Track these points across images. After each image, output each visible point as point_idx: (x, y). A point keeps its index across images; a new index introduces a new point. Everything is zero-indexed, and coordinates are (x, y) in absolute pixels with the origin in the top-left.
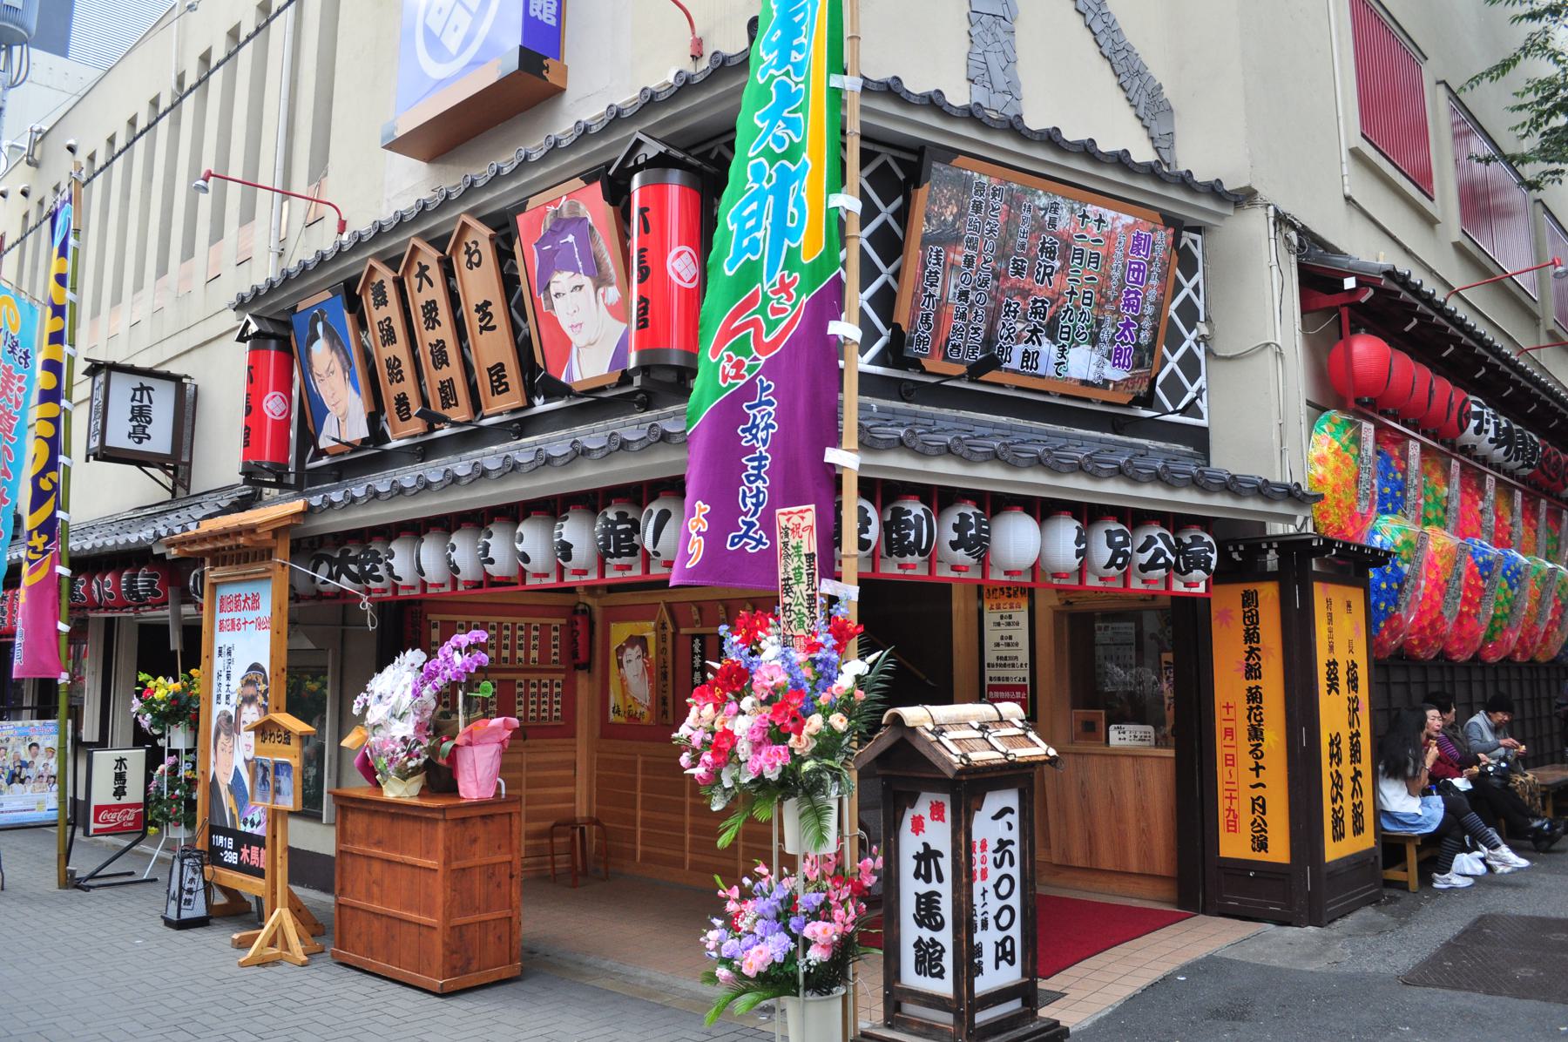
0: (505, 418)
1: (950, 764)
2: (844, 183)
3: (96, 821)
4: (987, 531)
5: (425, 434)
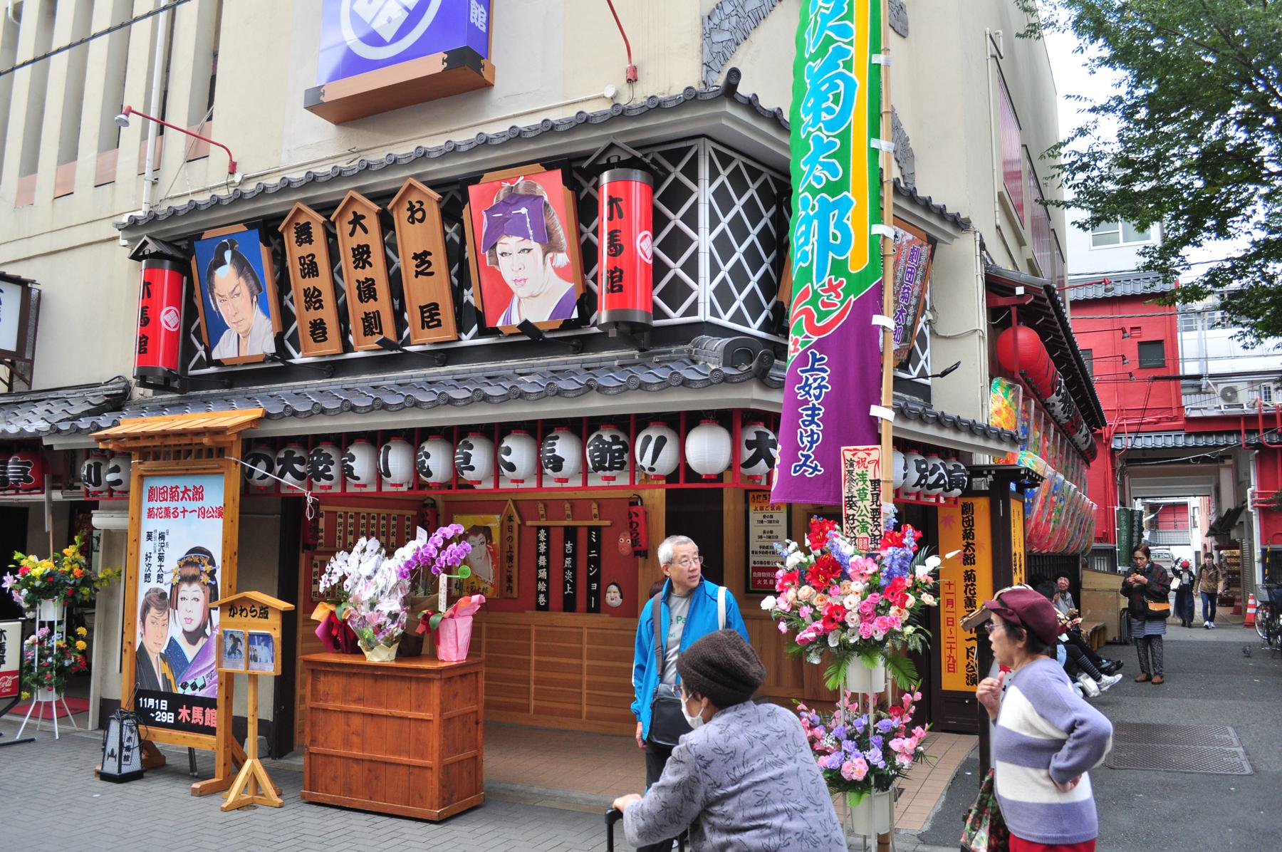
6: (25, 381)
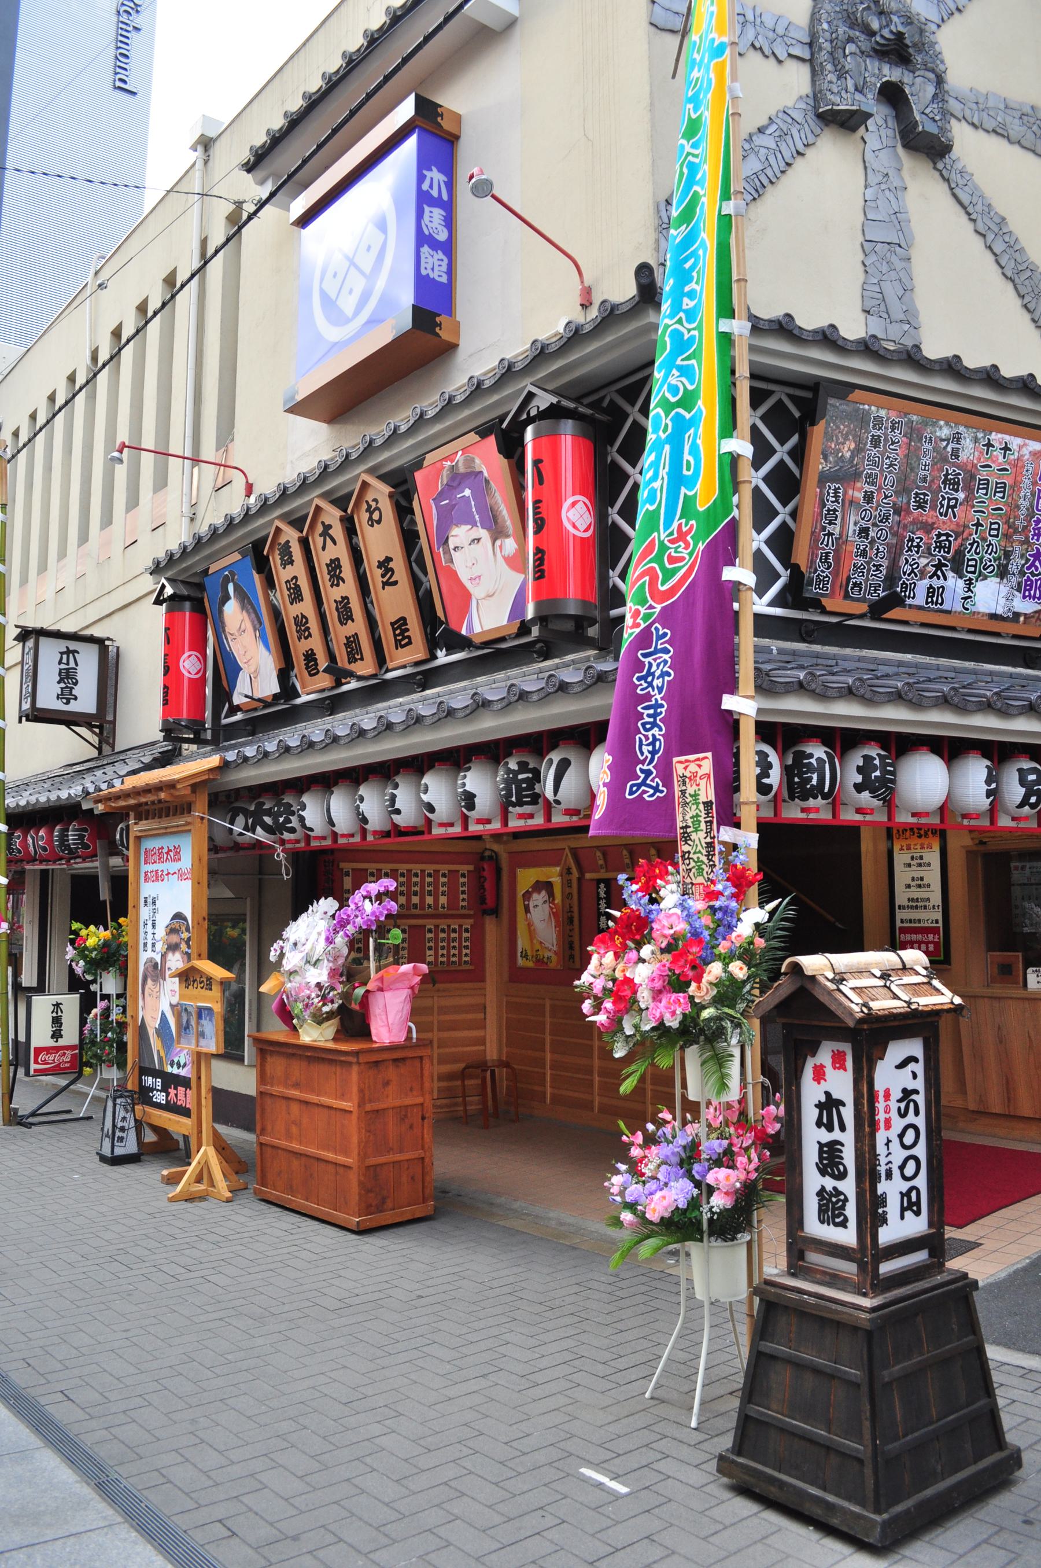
0: (409, 671)
1: (851, 1013)
2: (735, 427)
3: (36, 1062)
5: (332, 688)
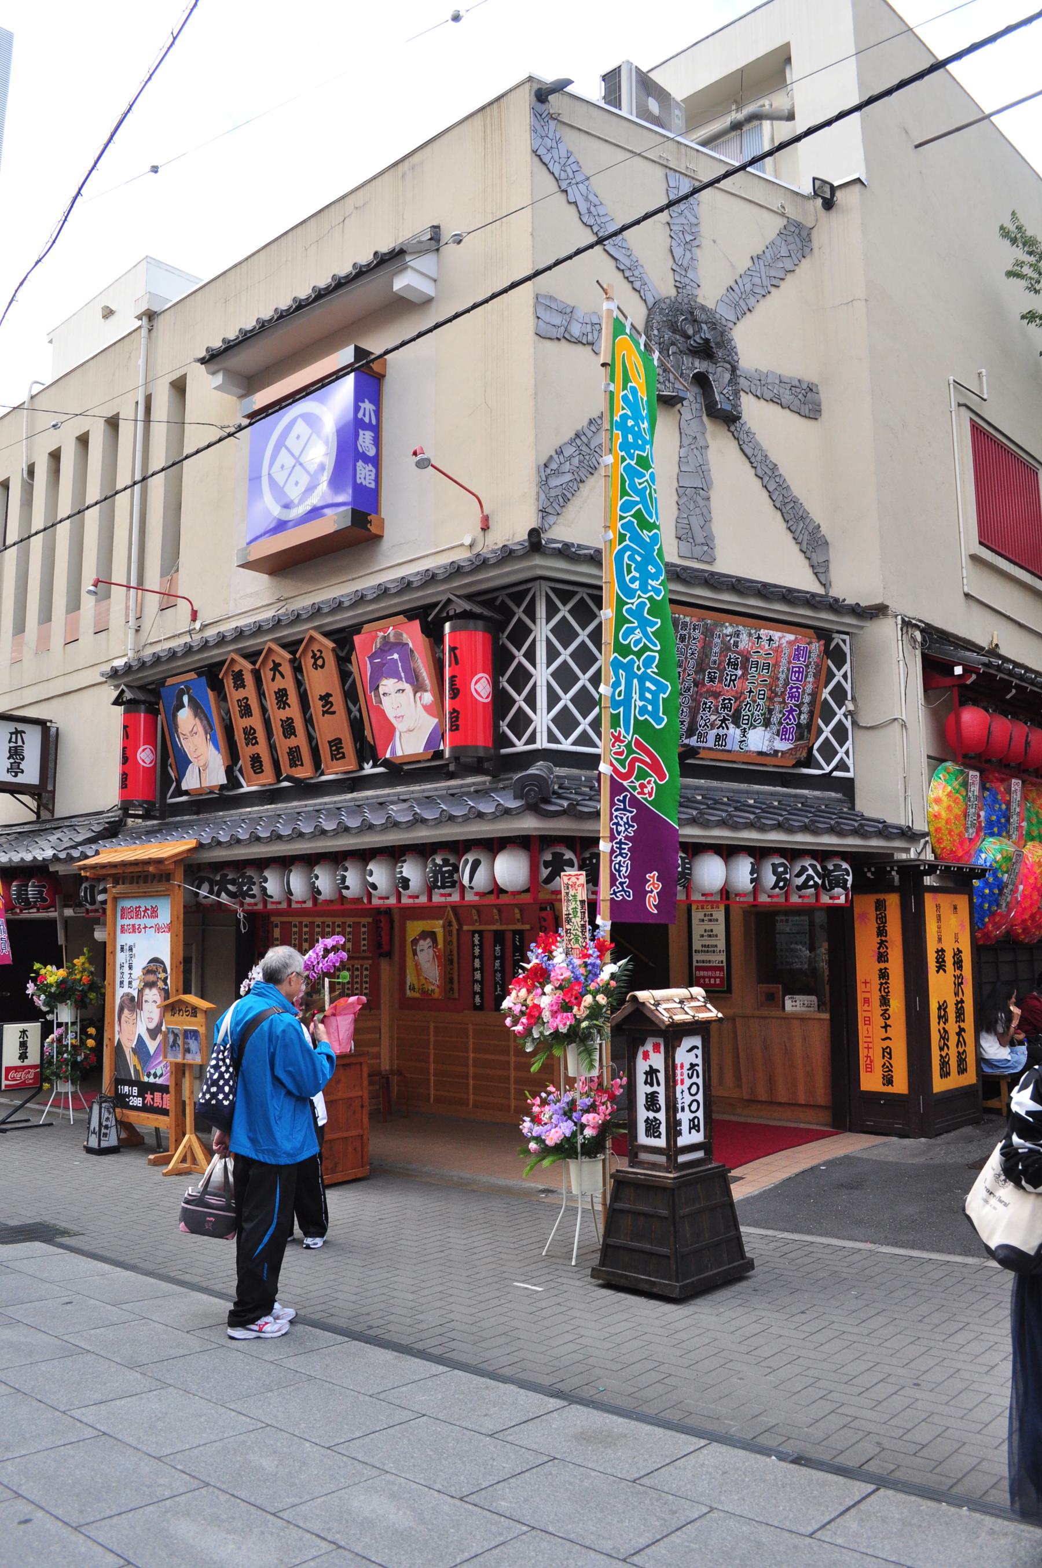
1: (663, 1022)
3: (7, 1079)
4: (690, 869)
6: (49, 810)
